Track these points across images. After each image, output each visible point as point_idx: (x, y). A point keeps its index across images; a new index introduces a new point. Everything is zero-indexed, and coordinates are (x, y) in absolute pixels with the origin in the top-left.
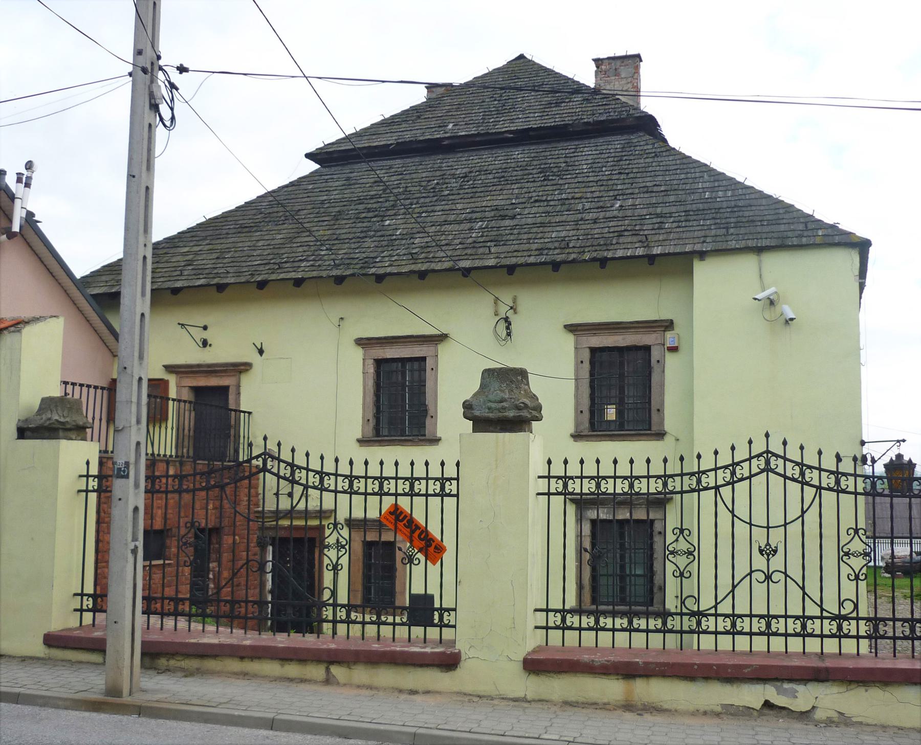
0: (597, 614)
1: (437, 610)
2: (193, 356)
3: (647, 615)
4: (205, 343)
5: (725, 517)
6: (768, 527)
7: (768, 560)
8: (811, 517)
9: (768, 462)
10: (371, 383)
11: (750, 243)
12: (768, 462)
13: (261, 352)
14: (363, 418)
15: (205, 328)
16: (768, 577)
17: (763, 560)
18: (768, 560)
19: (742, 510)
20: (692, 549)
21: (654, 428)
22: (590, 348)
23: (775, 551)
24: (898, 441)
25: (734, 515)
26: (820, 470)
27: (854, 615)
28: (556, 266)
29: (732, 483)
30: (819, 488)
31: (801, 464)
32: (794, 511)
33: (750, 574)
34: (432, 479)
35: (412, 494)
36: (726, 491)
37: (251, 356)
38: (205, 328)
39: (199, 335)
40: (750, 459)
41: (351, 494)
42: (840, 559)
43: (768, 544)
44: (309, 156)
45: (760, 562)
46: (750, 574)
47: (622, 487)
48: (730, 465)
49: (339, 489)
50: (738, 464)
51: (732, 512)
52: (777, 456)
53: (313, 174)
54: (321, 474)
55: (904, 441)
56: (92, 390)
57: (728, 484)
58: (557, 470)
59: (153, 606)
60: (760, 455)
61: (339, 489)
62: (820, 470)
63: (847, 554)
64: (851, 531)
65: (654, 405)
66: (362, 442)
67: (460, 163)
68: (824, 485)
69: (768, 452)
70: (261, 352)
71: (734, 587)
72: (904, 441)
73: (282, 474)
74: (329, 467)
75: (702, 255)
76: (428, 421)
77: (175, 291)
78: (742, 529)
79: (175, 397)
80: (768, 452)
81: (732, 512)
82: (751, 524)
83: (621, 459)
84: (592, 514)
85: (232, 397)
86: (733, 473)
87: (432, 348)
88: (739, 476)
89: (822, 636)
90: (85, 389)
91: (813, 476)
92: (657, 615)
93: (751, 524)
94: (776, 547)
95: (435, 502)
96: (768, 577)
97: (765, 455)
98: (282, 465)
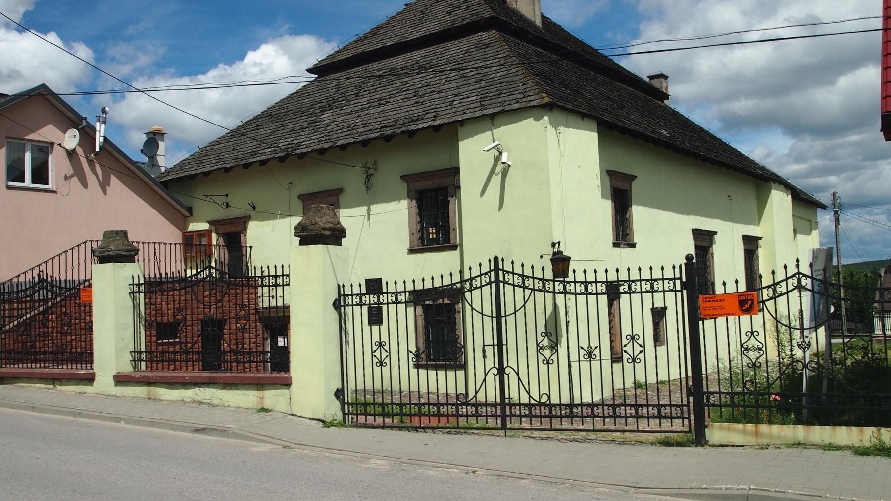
2: (220, 213)
4: (228, 205)
8: (530, 305)
9: (799, 281)
11: (486, 112)
12: (799, 281)
13: (254, 208)
15: (227, 195)
28: (388, 139)
29: (774, 298)
30: (533, 290)
32: (520, 304)
37: (249, 211)
38: (227, 195)
39: (222, 200)
40: (786, 279)
41: (586, 295)
42: (538, 351)
44: (309, 71)
49: (557, 290)
50: (778, 283)
54: (522, 276)
57: (771, 299)
59: (640, 411)
60: (794, 276)
61: (578, 292)
64: (749, 334)
67: (398, 61)
68: (536, 288)
69: (799, 273)
70: (254, 208)
73: (511, 275)
74: (528, 272)
75: (462, 123)
77: (206, 174)
80: (799, 273)
86: (774, 291)
91: (529, 283)
98: (516, 277)
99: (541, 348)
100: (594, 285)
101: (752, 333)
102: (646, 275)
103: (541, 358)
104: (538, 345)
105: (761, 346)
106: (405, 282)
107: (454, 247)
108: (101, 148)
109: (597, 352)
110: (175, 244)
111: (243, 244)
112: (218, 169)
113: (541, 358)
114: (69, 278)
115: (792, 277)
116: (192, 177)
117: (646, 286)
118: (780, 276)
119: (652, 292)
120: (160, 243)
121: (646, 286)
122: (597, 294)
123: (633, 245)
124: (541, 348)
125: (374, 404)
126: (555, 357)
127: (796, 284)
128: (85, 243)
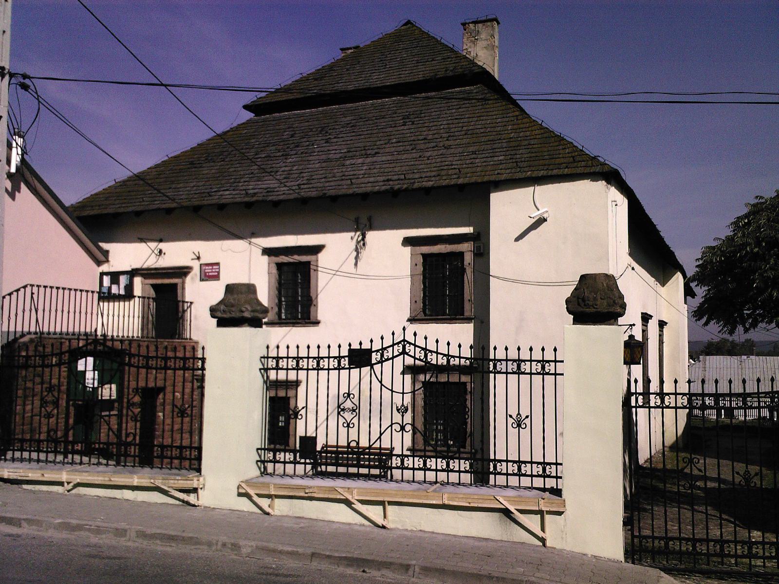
0: (425, 457)
1: (492, 460)
3: (285, 451)
5: (376, 385)
6: (403, 393)
7: (403, 416)
9: (404, 347)
10: (275, 284)
12: (404, 347)
14: (317, 307)
16: (403, 428)
17: (399, 416)
18: (403, 416)
19: (387, 382)
20: (355, 408)
21: (312, 319)
22: (422, 254)
23: (407, 410)
24: (631, 325)
25: (382, 385)
26: (437, 353)
27: (133, 442)
31: (425, 349)
33: (391, 426)
34: (270, 357)
35: (298, 368)
36: (377, 368)
42: (339, 413)
43: (403, 405)
44: (246, 107)
45: (397, 417)
46: (391, 426)
47: (442, 361)
48: (380, 350)
50: (385, 349)
51: (381, 382)
52: (410, 344)
53: (249, 122)
55: (634, 325)
56: (84, 294)
58: (273, 353)
60: (400, 342)
62: (437, 353)
63: (354, 411)
65: (313, 294)
66: (412, 320)
69: (404, 340)
71: (381, 434)
72: (634, 325)
76: (312, 309)
77: (138, 214)
78: (387, 394)
79: (140, 295)
80: (404, 340)
81: (381, 382)
82: (392, 391)
83: (452, 339)
84: (422, 377)
85: (179, 291)
86: (382, 355)
87: (315, 256)
88: (386, 358)
89: (507, 474)
90: (78, 293)
92: (290, 451)
93: (392, 391)
94: (407, 407)
95: (313, 373)
96: (403, 428)
97: (402, 343)
99: (343, 410)
100: (504, 363)
101: (348, 426)
102: (538, 355)
103: (341, 421)
104: (339, 407)
105: (342, 413)
106: (298, 347)
107: (317, 323)
108: (17, 168)
109: (303, 412)
110: (93, 292)
111: (179, 299)
112: (159, 209)
113: (341, 421)
114: (52, 330)
115: (398, 343)
116: (116, 216)
117: (512, 367)
118: (388, 342)
119: (543, 374)
120: (38, 286)
121: (512, 367)
122: (531, 374)
123: (317, 323)
124: (343, 410)
125: (707, 541)
126: (355, 421)
127: (400, 351)
128: (25, 287)
